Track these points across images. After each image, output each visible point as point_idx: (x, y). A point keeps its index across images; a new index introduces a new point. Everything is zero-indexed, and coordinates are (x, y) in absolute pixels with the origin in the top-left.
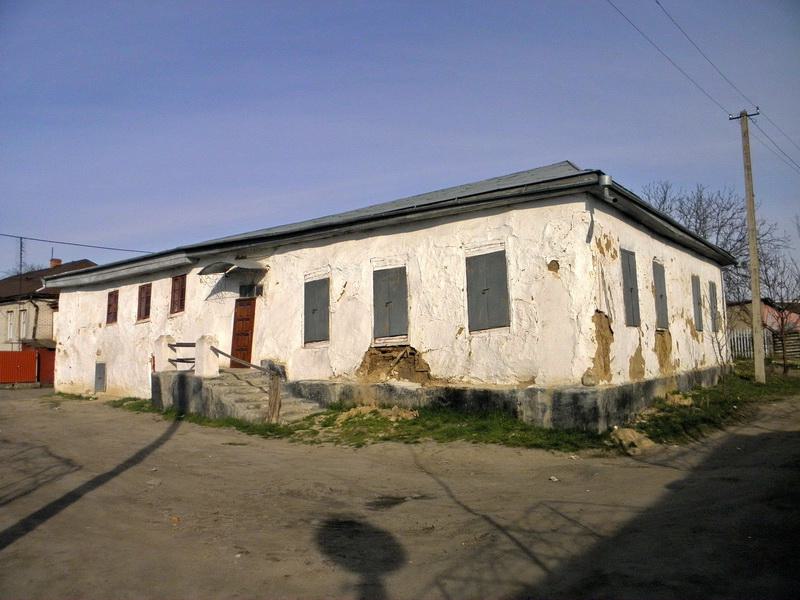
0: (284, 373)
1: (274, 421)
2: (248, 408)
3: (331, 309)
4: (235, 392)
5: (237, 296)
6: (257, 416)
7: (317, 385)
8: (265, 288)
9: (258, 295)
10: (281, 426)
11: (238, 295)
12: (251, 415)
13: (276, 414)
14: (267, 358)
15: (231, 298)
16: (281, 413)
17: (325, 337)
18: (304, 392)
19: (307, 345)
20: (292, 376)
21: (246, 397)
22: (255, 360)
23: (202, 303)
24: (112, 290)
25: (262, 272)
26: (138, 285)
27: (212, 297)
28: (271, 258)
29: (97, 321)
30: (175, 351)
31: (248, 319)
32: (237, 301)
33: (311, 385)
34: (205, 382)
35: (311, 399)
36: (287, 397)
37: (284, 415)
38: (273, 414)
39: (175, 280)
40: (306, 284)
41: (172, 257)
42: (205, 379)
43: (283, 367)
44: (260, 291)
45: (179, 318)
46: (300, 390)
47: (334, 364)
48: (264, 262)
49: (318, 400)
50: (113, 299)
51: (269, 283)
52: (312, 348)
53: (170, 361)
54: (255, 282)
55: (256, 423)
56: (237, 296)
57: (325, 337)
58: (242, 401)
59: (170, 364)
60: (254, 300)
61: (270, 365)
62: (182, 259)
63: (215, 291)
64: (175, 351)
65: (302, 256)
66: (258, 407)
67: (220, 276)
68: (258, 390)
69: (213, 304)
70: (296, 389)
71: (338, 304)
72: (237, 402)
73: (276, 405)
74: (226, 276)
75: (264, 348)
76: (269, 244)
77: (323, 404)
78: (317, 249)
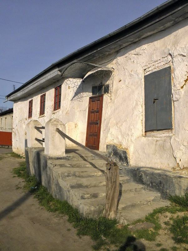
0: (126, 158)
1: (112, 215)
2: (83, 198)
3: (175, 97)
4: (74, 175)
5: (90, 95)
6: (93, 208)
7: (159, 175)
8: (111, 86)
9: (105, 93)
10: (119, 226)
11: (91, 94)
12: (85, 207)
13: (114, 209)
14: (112, 143)
15: (87, 96)
16: (121, 206)
17: (168, 126)
18: (145, 179)
19: (148, 133)
20: (133, 162)
21: (84, 181)
22: (102, 148)
23: (69, 102)
24: (30, 100)
25: (108, 74)
26: (40, 95)
27: (75, 98)
28: (114, 61)
29: (25, 117)
30: (41, 132)
31: (98, 112)
32: (90, 98)
33: (153, 174)
34: (49, 162)
35: (152, 187)
36: (128, 181)
37: (124, 209)
38: (110, 208)
39: (56, 89)
40: (146, 77)
41: (51, 72)
42: (51, 158)
43: (125, 153)
44: (107, 90)
45: (58, 113)
46: (141, 176)
47: (178, 155)
48: (110, 66)
49: (159, 190)
50: (31, 103)
51: (114, 83)
52: (153, 136)
53: (37, 139)
54: (103, 83)
55: (91, 216)
56: (90, 95)
57: (168, 126)
58: (79, 186)
59: (37, 142)
60: (102, 96)
61: (114, 150)
62: (55, 73)
63: (76, 94)
64: (41, 132)
65: (141, 52)
66: (95, 196)
67: (79, 81)
68: (100, 173)
69: (76, 102)
70: (137, 175)
71: (182, 91)
72: (72, 187)
73: (117, 192)
74: (83, 81)
75: (109, 135)
76: (112, 46)
77: (165, 196)
78: (156, 43)
